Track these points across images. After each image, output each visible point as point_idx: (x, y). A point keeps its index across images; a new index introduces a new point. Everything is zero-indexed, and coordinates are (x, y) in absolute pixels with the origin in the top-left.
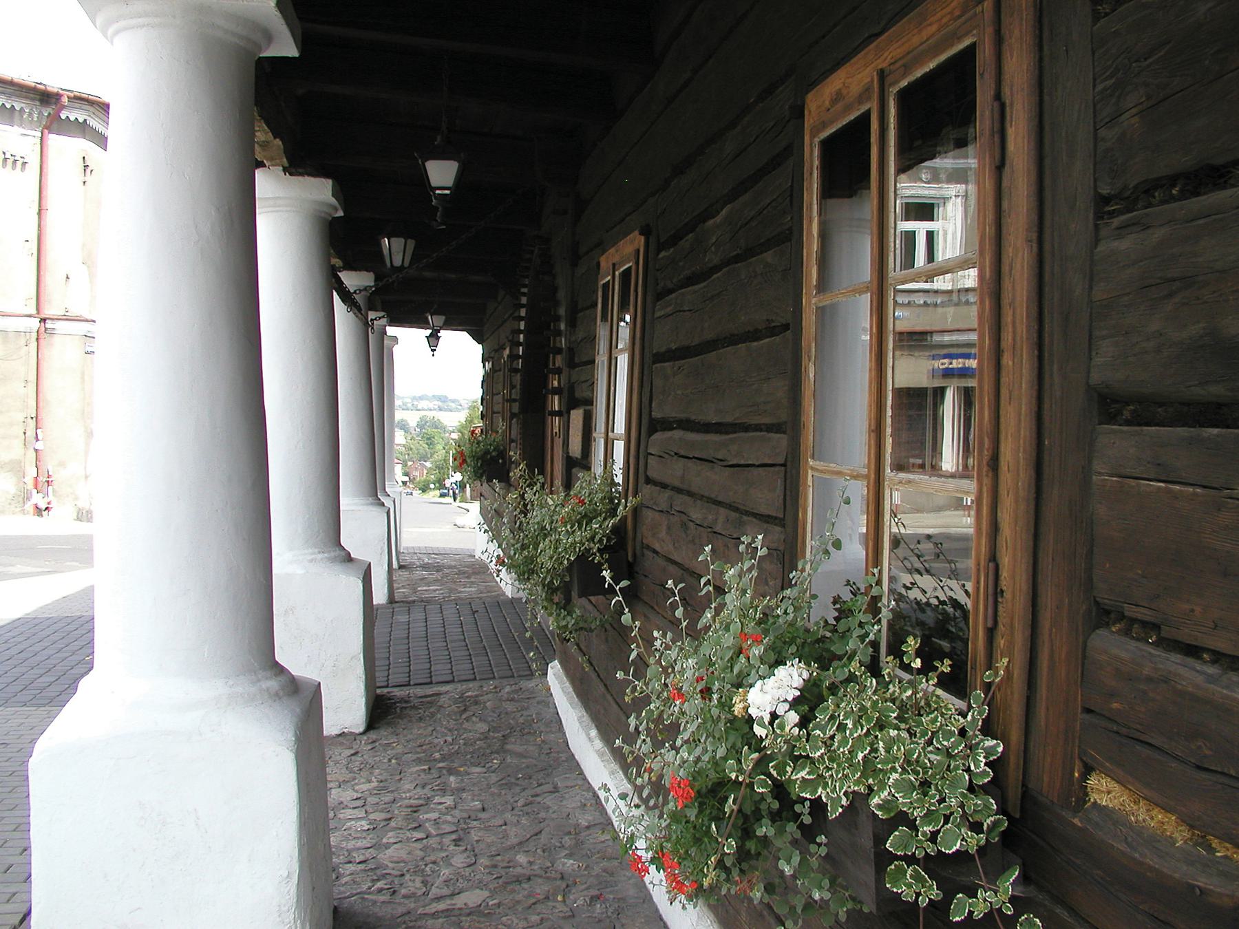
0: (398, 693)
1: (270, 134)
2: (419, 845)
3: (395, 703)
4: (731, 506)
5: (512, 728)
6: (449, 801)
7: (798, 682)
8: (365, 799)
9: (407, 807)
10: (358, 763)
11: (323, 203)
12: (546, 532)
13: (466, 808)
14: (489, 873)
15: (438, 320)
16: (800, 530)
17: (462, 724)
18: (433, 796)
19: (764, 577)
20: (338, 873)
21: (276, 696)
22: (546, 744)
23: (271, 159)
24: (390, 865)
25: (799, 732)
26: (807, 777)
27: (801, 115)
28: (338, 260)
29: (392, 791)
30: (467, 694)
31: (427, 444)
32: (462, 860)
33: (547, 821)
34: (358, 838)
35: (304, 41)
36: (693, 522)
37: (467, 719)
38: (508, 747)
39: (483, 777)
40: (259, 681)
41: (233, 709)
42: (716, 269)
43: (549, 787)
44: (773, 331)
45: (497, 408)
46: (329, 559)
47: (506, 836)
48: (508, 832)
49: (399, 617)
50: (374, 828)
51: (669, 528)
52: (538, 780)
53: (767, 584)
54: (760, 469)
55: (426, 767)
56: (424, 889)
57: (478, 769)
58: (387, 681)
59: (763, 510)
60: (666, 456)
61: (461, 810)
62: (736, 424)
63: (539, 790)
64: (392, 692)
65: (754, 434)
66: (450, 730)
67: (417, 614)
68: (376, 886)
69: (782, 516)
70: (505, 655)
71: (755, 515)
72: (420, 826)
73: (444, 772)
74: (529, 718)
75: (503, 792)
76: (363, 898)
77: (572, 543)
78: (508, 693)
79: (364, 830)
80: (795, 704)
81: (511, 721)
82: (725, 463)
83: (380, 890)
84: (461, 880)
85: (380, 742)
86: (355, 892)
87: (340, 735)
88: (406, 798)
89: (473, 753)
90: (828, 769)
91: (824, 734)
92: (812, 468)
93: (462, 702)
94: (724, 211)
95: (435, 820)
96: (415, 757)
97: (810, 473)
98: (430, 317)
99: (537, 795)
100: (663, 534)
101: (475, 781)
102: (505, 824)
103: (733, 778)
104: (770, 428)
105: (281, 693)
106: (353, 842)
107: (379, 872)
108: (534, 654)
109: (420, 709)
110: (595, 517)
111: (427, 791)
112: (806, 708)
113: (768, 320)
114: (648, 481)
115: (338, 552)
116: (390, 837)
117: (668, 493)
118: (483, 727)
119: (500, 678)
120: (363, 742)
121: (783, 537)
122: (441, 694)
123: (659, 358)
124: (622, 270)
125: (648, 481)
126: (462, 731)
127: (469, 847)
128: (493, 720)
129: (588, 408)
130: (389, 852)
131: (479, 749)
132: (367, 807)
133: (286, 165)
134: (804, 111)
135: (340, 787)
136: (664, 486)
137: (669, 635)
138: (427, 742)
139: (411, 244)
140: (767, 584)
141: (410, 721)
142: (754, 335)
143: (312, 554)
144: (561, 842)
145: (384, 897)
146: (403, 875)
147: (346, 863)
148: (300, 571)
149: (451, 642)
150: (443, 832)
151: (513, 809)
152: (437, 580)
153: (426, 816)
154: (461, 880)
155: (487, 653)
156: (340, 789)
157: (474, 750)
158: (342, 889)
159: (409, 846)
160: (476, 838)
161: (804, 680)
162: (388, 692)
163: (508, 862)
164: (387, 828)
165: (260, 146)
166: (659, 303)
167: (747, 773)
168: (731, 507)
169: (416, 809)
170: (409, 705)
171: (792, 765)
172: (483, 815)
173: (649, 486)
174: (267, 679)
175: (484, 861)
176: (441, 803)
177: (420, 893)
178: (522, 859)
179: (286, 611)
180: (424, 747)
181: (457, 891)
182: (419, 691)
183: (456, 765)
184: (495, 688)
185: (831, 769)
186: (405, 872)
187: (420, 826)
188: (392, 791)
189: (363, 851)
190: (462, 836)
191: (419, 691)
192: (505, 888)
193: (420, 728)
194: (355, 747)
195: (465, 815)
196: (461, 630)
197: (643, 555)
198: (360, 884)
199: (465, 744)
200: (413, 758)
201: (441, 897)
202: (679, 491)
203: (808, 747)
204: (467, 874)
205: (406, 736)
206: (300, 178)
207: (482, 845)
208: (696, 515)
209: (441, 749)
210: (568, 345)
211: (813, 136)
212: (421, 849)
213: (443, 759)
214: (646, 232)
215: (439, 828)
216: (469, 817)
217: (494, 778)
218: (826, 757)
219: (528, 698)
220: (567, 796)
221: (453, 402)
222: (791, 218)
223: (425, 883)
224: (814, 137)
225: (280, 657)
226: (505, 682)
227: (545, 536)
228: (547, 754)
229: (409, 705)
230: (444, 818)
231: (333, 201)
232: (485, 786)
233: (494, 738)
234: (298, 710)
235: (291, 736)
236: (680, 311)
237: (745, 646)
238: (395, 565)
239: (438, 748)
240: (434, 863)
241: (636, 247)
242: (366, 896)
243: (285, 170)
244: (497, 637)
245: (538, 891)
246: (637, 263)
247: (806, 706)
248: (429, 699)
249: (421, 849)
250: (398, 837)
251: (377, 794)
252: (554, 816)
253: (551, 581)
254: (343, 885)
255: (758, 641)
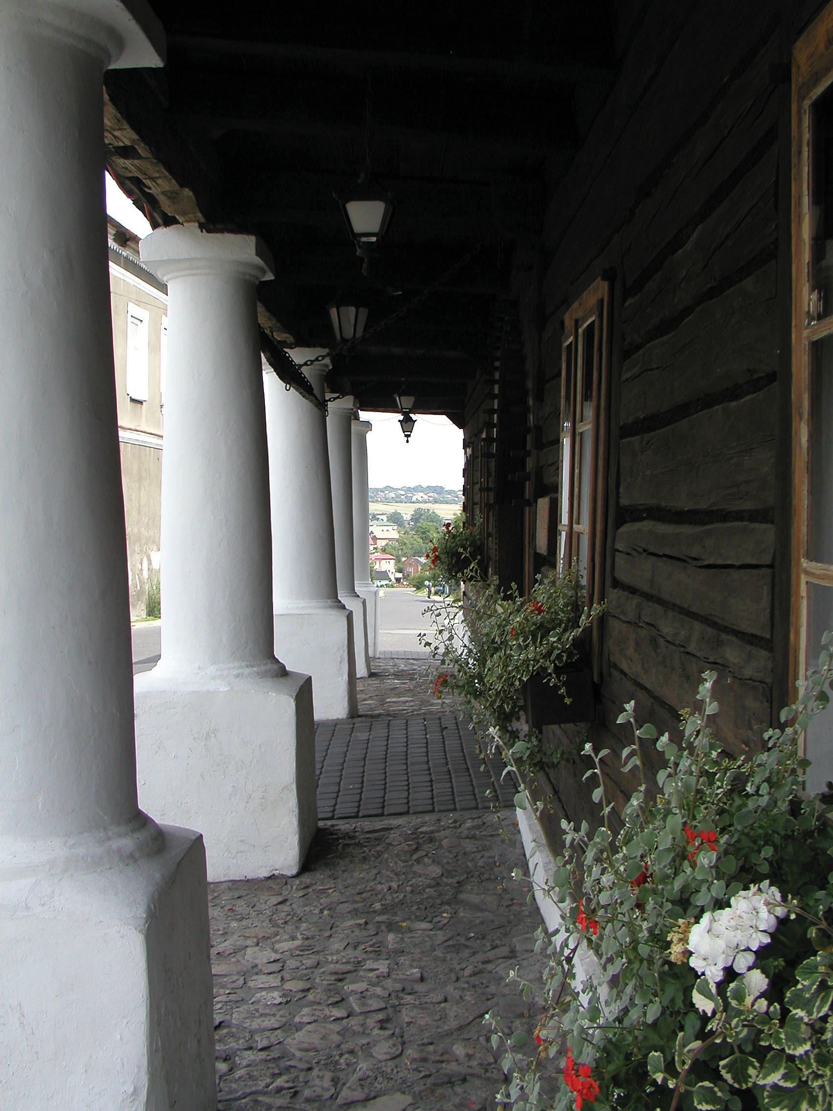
0: (344, 826)
1: (174, 181)
2: (336, 1027)
3: (338, 839)
4: (707, 619)
5: (470, 872)
6: (382, 966)
7: (766, 920)
8: (285, 962)
9: (331, 974)
10: (284, 914)
11: (245, 264)
12: (495, 645)
13: (402, 977)
14: (417, 1070)
15: (406, 402)
16: (791, 659)
17: (411, 866)
18: (364, 960)
19: (747, 717)
20: (234, 1062)
21: (131, 858)
22: (508, 893)
23: (184, 214)
24: (298, 1054)
25: (768, 1008)
26: (782, 1083)
27: (788, 78)
28: (288, 335)
29: (318, 952)
30: (421, 830)
31: (422, 538)
32: (386, 1050)
33: (495, 999)
34: (265, 1015)
35: (169, 53)
36: (664, 638)
37: (418, 861)
38: (462, 896)
39: (428, 936)
40: (109, 839)
41: (72, 875)
42: (687, 311)
43: (504, 951)
44: (755, 385)
45: (477, 498)
46: (257, 673)
47: (443, 1018)
48: (447, 1011)
49: (358, 734)
50: (287, 1002)
51: (637, 644)
52: (493, 941)
53: (751, 729)
54: (742, 571)
55: (362, 921)
56: (333, 1091)
57: (424, 925)
58: (334, 811)
59: (745, 627)
60: (634, 553)
61: (395, 980)
62: (712, 511)
63: (491, 955)
64: (336, 825)
65: (736, 524)
66: (396, 874)
67: (379, 731)
68: (274, 1085)
69: (768, 637)
70: (471, 781)
71: (738, 634)
72: (343, 1000)
73: (383, 927)
74: (491, 860)
75: (448, 958)
76: (256, 1101)
77: (524, 661)
78: (468, 829)
79: (275, 1004)
80: (762, 956)
81: (469, 864)
82: (700, 563)
83: (279, 1090)
84: (380, 1079)
85: (314, 887)
86: (248, 1091)
87: (270, 878)
88: (331, 962)
89: (420, 903)
90: (817, 1076)
91: (810, 1013)
92: (807, 573)
93: (414, 839)
94: (695, 235)
95: (361, 993)
96: (351, 907)
97: (803, 579)
98: (397, 398)
99: (488, 962)
100: (630, 651)
101: (417, 941)
102: (446, 1000)
103: (659, 1081)
104: (754, 516)
105: (137, 855)
106: (259, 1020)
107: (284, 1063)
108: (491, 792)
109: (365, 846)
110: (554, 629)
111: (359, 953)
112: (781, 962)
113: (749, 370)
114: (616, 584)
115: (270, 666)
116: (304, 1015)
117: (636, 600)
118: (435, 871)
119: (462, 810)
120: (294, 887)
121: (770, 666)
122: (392, 829)
123: (627, 431)
124: (585, 326)
125: (616, 584)
126: (410, 876)
127: (397, 1030)
128: (448, 863)
129: (554, 495)
130: (300, 1035)
131: (427, 898)
132: (284, 973)
133: (203, 220)
134: (790, 69)
135: (258, 944)
136: (633, 591)
137: (584, 825)
138: (368, 889)
139: (364, 313)
140: (751, 729)
141: (351, 862)
142: (733, 393)
143: (239, 668)
144: (510, 1028)
145: (282, 1101)
146: (310, 1069)
147: (246, 1049)
148: (224, 688)
149: (413, 764)
150: (368, 1009)
151: (458, 979)
152: (410, 690)
153: (352, 987)
154: (380, 1079)
155: (451, 778)
156: (258, 948)
157: (422, 900)
158: (234, 1086)
159: (325, 1028)
160: (407, 1019)
161: (777, 917)
162: (333, 826)
163: (442, 1055)
164: (304, 1002)
165: (169, 198)
166: (625, 363)
167: (683, 1074)
168: (706, 620)
169: (341, 976)
170: (353, 842)
171: (757, 1065)
172: (420, 988)
173: (615, 591)
174: (120, 836)
175: (411, 1052)
176: (372, 970)
177: (327, 1095)
178: (459, 1050)
179: (208, 734)
180: (364, 895)
181: (372, 1094)
182: (367, 824)
183: (397, 918)
184: (455, 822)
185: (822, 1076)
186: (314, 1065)
187: (343, 1000)
188: (318, 952)
189: (268, 1033)
190: (391, 1015)
191: (367, 824)
192: (433, 1091)
193: (362, 871)
194: (285, 893)
195: (398, 986)
196: (425, 750)
197: (610, 675)
198: (256, 1080)
199: (412, 892)
200: (348, 910)
201: (353, 1102)
202: (648, 597)
203: (782, 1036)
204: (389, 1071)
205: (345, 881)
206: (219, 235)
207: (413, 1030)
208: (667, 629)
209: (384, 898)
210: (536, 423)
211: (802, 98)
212: (338, 1033)
213: (385, 910)
214: (610, 276)
215: (364, 1005)
216: (403, 990)
217: (440, 936)
218: (812, 1056)
219: (491, 836)
220: (525, 963)
221: (449, 494)
222: (776, 227)
223: (335, 1081)
224: (803, 99)
225: (143, 805)
226: (467, 814)
227: (496, 650)
228: (508, 906)
229: (353, 842)
230: (372, 989)
231: (258, 261)
232: (428, 947)
233: (447, 885)
234: (158, 876)
235: (141, 912)
236: (647, 370)
237: (690, 849)
238: (361, 670)
239: (380, 896)
240: (351, 1052)
241: (600, 297)
242: (260, 1099)
243: (202, 227)
244: (465, 760)
245: (473, 1098)
246: (601, 315)
247: (781, 959)
248: (377, 835)
249: (338, 1033)
250: (313, 1015)
251: (298, 955)
252: (506, 991)
253: (501, 707)
254: (236, 1081)
255: (711, 842)
